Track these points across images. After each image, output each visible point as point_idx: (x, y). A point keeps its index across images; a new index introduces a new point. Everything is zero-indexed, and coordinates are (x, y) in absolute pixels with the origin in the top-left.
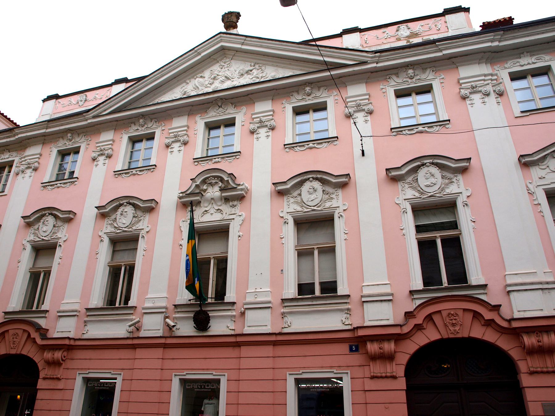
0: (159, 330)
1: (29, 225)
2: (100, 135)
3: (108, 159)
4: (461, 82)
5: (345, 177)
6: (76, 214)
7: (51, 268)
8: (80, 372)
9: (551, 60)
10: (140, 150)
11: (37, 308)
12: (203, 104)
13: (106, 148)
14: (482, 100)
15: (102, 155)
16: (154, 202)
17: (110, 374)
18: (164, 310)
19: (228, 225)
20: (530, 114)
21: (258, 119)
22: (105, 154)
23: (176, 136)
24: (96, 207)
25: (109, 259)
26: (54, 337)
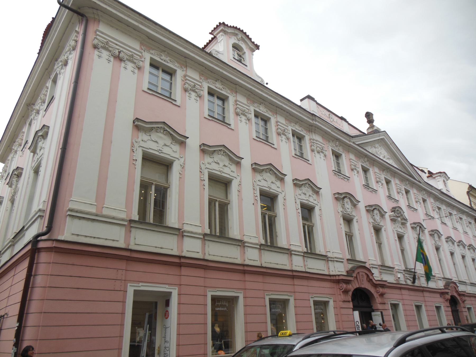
4: (98, 33)
8: (209, 290)
9: (178, 67)
13: (134, 56)
14: (133, 69)
17: (234, 293)
20: (298, 158)
21: (131, 53)
23: (132, 56)
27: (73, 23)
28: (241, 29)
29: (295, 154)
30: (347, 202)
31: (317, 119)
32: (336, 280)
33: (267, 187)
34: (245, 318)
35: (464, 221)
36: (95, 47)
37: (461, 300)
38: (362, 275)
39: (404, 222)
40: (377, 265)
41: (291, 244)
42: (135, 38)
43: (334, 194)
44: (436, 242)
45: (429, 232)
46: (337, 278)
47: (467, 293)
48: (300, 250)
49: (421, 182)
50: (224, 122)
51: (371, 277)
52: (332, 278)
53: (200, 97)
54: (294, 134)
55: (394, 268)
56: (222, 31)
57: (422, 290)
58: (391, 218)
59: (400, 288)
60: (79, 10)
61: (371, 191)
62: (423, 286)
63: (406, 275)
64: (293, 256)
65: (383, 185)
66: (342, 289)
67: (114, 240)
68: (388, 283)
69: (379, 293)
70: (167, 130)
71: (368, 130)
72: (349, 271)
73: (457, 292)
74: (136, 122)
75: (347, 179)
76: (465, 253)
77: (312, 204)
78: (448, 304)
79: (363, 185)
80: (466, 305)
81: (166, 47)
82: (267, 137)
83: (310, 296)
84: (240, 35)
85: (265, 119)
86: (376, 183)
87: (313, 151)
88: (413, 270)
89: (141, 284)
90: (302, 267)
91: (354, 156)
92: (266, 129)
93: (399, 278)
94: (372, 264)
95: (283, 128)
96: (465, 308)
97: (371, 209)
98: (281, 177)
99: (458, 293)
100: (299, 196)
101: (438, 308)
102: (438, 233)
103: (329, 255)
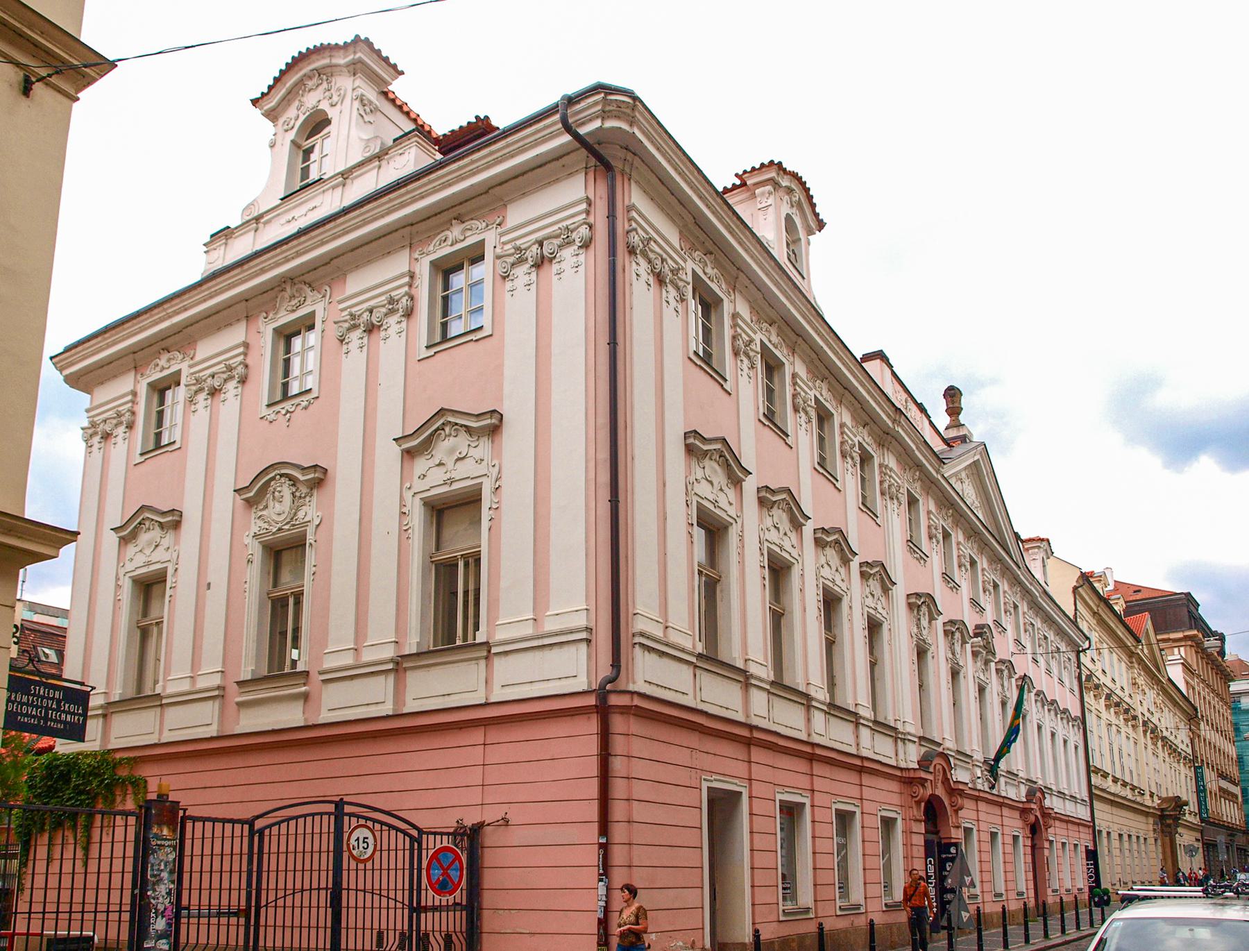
1: (250, 503)
3: (584, 250)
5: (171, 513)
6: (326, 470)
7: (480, 546)
10: (461, 290)
11: (465, 638)
12: (150, 346)
16: (496, 415)
18: (216, 693)
19: (479, 487)
20: (768, 426)
24: (394, 440)
26: (404, 712)
28: (811, 193)
29: (696, 353)
30: (924, 614)
32: (909, 778)
34: (1004, 858)
36: (632, 251)
39: (887, 584)
40: (914, 736)
41: (747, 657)
42: (671, 217)
43: (908, 595)
45: (861, 565)
47: (1056, 813)
48: (687, 643)
54: (700, 289)
56: (772, 181)
58: (975, 649)
60: (596, 147)
61: (951, 588)
64: (812, 709)
70: (725, 456)
77: (787, 556)
81: (716, 245)
85: (709, 299)
94: (642, 634)
95: (675, 266)
101: (888, 823)
102: (1011, 670)
103: (899, 726)
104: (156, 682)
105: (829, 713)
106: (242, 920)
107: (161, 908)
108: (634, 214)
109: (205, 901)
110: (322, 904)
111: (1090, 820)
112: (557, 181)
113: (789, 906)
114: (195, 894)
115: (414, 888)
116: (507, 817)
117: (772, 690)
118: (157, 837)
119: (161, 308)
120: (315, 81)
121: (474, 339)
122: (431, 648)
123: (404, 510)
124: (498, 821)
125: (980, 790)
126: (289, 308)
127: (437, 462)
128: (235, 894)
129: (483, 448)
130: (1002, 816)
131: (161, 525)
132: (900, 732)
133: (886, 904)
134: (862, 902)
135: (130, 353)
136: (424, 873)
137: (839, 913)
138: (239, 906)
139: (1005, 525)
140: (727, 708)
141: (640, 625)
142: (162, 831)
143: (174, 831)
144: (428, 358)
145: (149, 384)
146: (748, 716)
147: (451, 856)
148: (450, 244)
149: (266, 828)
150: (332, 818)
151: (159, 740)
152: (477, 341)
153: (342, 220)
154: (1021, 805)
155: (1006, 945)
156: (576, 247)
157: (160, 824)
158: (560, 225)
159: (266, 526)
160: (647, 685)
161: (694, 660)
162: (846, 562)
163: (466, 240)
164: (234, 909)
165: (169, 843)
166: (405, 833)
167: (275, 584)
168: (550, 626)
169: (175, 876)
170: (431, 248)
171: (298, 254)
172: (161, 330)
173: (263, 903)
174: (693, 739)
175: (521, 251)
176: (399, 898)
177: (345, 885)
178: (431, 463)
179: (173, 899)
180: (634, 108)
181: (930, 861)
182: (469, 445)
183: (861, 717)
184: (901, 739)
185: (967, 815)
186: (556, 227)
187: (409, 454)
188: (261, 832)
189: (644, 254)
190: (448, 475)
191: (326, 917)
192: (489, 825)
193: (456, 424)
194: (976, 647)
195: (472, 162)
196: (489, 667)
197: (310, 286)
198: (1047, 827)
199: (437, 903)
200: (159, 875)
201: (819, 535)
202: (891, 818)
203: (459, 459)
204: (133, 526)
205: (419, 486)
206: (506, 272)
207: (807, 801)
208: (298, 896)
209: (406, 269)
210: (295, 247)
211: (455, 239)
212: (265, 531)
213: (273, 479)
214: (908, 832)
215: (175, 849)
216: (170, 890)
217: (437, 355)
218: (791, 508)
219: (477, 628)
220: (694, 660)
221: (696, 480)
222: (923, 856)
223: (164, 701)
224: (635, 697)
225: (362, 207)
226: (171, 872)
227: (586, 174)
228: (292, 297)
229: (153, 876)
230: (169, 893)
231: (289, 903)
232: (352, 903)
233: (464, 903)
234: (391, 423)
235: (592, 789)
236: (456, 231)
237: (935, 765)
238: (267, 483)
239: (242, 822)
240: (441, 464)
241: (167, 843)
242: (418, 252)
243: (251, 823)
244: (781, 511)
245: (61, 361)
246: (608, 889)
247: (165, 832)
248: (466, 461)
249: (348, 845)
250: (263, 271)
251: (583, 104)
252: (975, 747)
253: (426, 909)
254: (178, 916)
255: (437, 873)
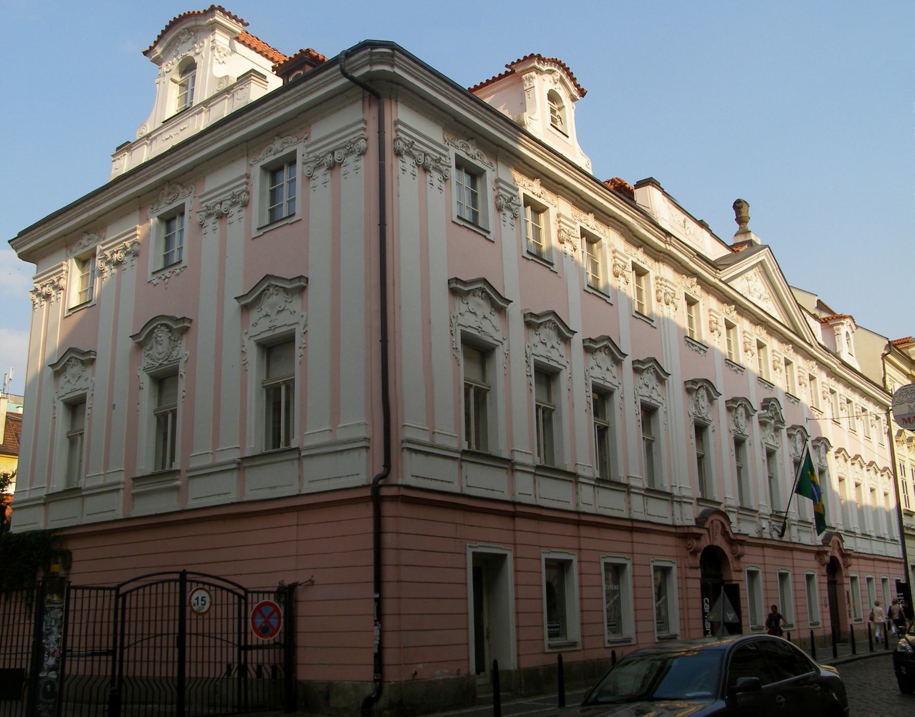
0: (114, 510)
2: (204, 182)
7: (294, 375)
15: (319, 166)
16: (303, 280)
22: (324, 164)
23: (234, 196)
24: (130, 337)
25: (155, 406)
27: (347, 97)
30: (703, 396)
31: (673, 241)
33: (601, 378)
35: (653, 282)
36: (398, 154)
37: (733, 554)
38: (717, 526)
41: (513, 448)
43: (685, 382)
44: (820, 460)
46: (686, 530)
48: (454, 445)
49: (814, 345)
50: (475, 224)
51: (728, 529)
52: (679, 530)
53: (445, 180)
55: (756, 511)
57: (792, 548)
58: (761, 420)
59: (763, 546)
60: (368, 84)
61: (735, 370)
62: (859, 551)
63: (773, 523)
64: (632, 495)
65: (722, 335)
66: (691, 548)
67: (417, 477)
68: (751, 537)
69: (735, 554)
70: (486, 292)
71: (736, 237)
72: (699, 518)
73: (840, 550)
74: (453, 283)
75: (704, 350)
76: (845, 473)
78: (824, 570)
79: (726, 359)
80: (850, 572)
82: (475, 214)
83: (468, 544)
84: (559, 73)
86: (496, 211)
87: (659, 301)
88: (784, 515)
89: (479, 544)
90: (530, 495)
91: (441, 128)
92: (474, 196)
93: (764, 528)
94: (409, 441)
96: (848, 577)
97: (733, 405)
98: (565, 335)
99: (842, 552)
100: (639, 389)
101: (809, 578)
103: (676, 492)
104: (79, 478)
105: (598, 486)
106: (110, 658)
107: (52, 650)
108: (400, 127)
109: (83, 644)
110: (171, 644)
111: (902, 557)
112: (345, 106)
113: (614, 637)
114: (76, 640)
115: (242, 632)
116: (313, 578)
117: (537, 473)
118: (50, 602)
119: (81, 205)
120: (186, 36)
121: (290, 222)
122: (264, 451)
123: (244, 349)
124: (306, 582)
125: (766, 539)
126: (168, 202)
127: (265, 314)
128: (105, 639)
129: (296, 304)
130: (793, 559)
131: (83, 362)
132: (675, 496)
133: (609, 641)
134: (633, 635)
135: (135, 198)
136: (250, 621)
137: (547, 650)
138: (108, 647)
139: (794, 311)
140: (493, 490)
141: (409, 434)
142: (53, 598)
143: (62, 597)
144: (259, 236)
145: (263, 167)
146: (513, 495)
147: (271, 609)
148: (273, 153)
149: (128, 592)
150: (178, 584)
151: (300, 491)
152: (291, 224)
153: (199, 140)
154: (816, 549)
155: (81, 715)
156: (356, 155)
157: (52, 594)
158: (345, 140)
159: (150, 362)
160: (414, 479)
161: (459, 456)
162: (618, 362)
163: (284, 150)
164: (104, 649)
165: (59, 606)
166: (235, 593)
167: (268, 375)
168: (341, 436)
169: (62, 630)
170: (261, 157)
171: (172, 165)
172: (82, 220)
173: (126, 644)
174: (458, 516)
175: (320, 159)
176: (230, 640)
177: (188, 631)
178: (260, 314)
179: (61, 644)
180: (393, 55)
181: (706, 601)
182: (286, 301)
183: (632, 487)
184: (677, 501)
185: (751, 559)
186: (342, 141)
187: (246, 308)
188: (124, 595)
189: (409, 154)
190: (272, 324)
191: (174, 654)
192: (300, 585)
193: (277, 286)
194: (763, 417)
195: (285, 98)
196: (301, 466)
197: (181, 185)
198: (847, 566)
199: (260, 643)
200: (51, 629)
201: (587, 344)
202: (666, 567)
203: (279, 312)
204: (63, 363)
205: (253, 331)
206: (309, 174)
207: (575, 559)
208: (158, 639)
209: (244, 173)
210: (169, 160)
211: (278, 149)
212: (151, 366)
213: (156, 327)
214: (683, 578)
215: (62, 609)
216: (59, 639)
217: (266, 235)
218: (557, 326)
219: (173, 459)
220: (459, 456)
221: (460, 314)
222: (700, 596)
223: (84, 493)
224: (402, 489)
225: (213, 131)
226: (59, 627)
227: (363, 101)
228: (169, 194)
229: (47, 630)
230: (58, 641)
231: (152, 644)
232: (194, 644)
233: (282, 642)
234: (238, 285)
235: (370, 558)
236: (277, 145)
237: (712, 522)
238: (152, 332)
239: (111, 589)
240: (267, 315)
241: (56, 606)
242: (252, 160)
243: (117, 589)
244: (548, 329)
245: (16, 243)
246: (382, 631)
247: (56, 598)
248: (284, 312)
249: (190, 603)
250: (149, 177)
251: (356, 56)
252: (761, 503)
253: (251, 648)
254: (63, 656)
255: (259, 621)
